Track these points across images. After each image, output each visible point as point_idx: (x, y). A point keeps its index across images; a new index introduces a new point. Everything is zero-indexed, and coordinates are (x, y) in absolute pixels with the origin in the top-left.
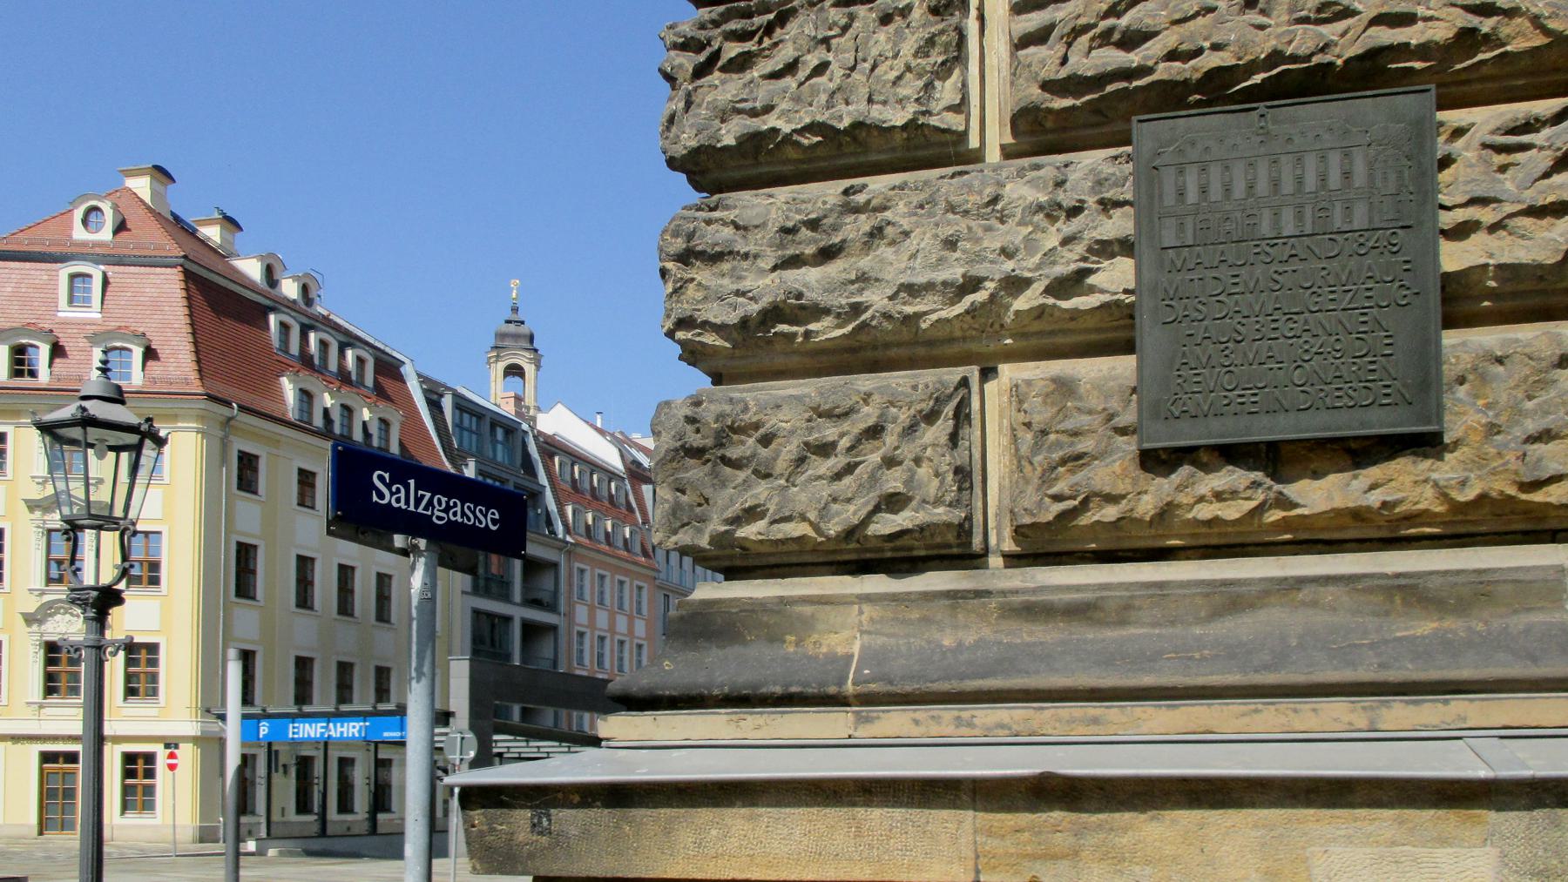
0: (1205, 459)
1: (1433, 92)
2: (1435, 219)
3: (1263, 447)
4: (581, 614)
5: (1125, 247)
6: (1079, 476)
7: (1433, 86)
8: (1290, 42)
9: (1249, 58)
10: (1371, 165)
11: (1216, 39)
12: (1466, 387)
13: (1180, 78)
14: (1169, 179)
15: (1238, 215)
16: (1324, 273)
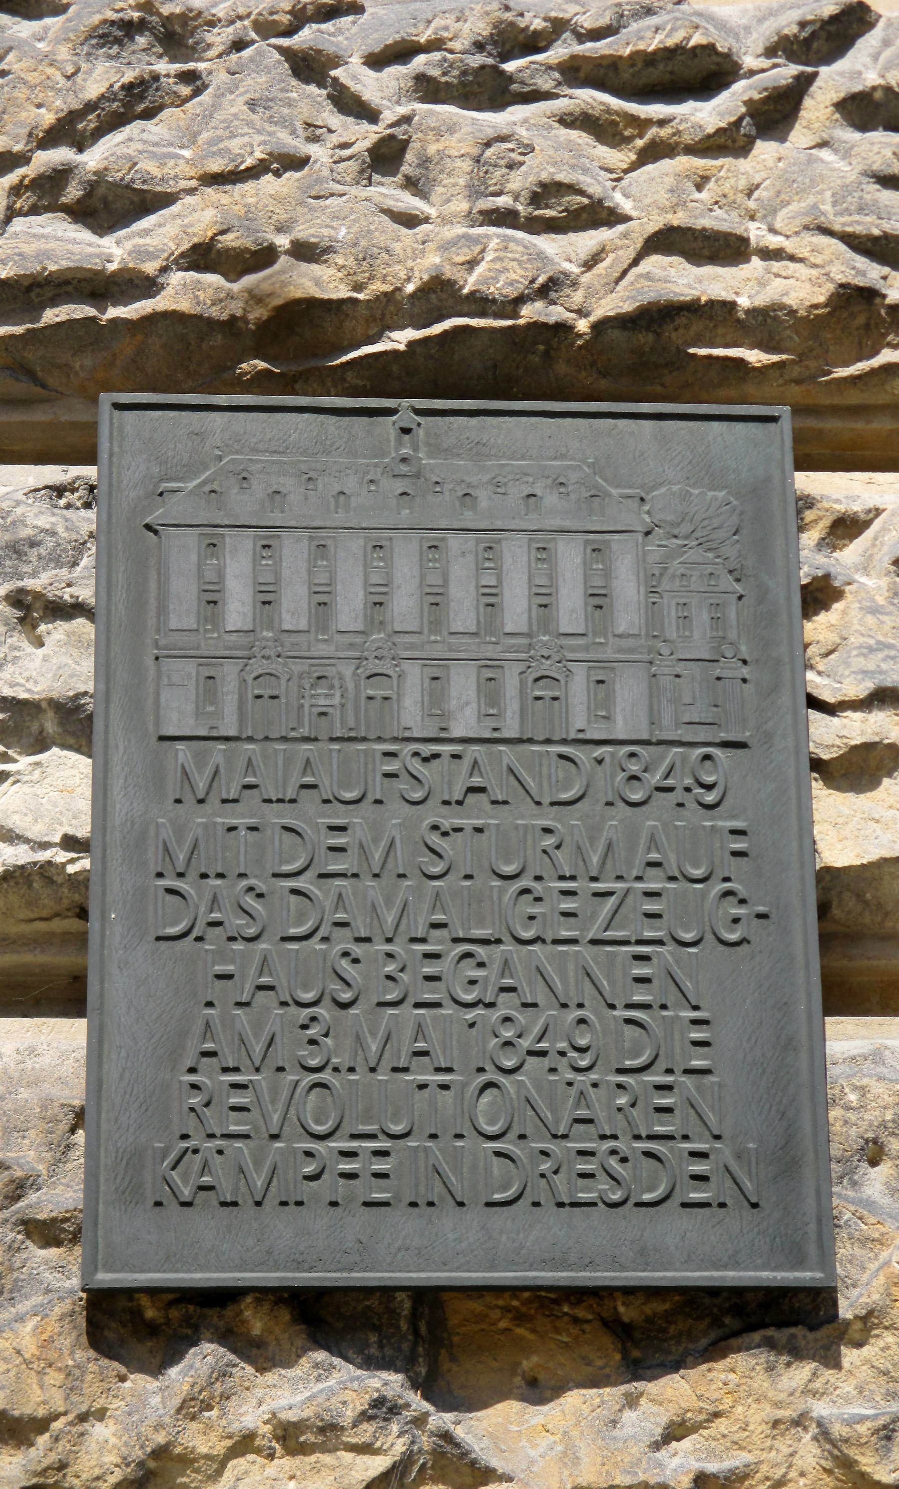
0: (257, 1327)
1: (786, 425)
2: (802, 732)
3: (405, 1304)
4: (339, 587)
5: (70, 723)
7: (784, 411)
8: (472, 264)
9: (378, 287)
11: (304, 232)
12: (885, 1169)
14: (183, 553)
15: (347, 670)
16: (549, 841)
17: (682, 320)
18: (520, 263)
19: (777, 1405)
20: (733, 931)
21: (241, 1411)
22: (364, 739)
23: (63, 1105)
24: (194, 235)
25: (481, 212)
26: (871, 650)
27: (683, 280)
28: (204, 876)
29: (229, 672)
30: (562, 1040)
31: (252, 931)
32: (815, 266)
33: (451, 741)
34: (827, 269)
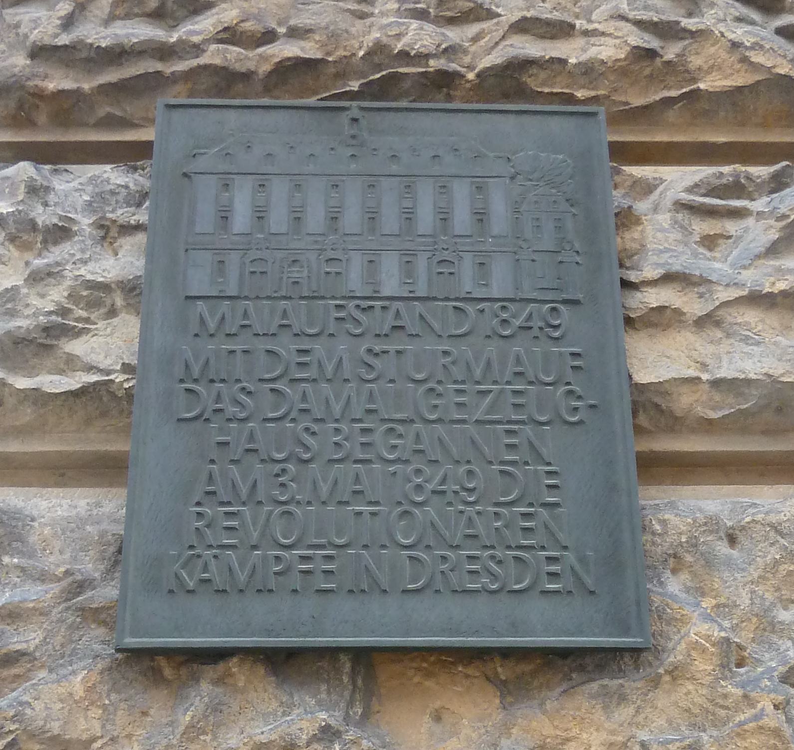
8: (399, 36)
9: (341, 53)
14: (206, 190)
15: (313, 256)
17: (534, 70)
18: (430, 36)
19: (613, 732)
20: (574, 416)
21: (228, 736)
22: (323, 298)
23: (114, 535)
24: (225, 22)
25: (406, 10)
26: (661, 252)
28: (212, 381)
29: (234, 258)
30: (456, 485)
31: (243, 415)
32: (617, 37)
33: (380, 299)
34: (625, 38)
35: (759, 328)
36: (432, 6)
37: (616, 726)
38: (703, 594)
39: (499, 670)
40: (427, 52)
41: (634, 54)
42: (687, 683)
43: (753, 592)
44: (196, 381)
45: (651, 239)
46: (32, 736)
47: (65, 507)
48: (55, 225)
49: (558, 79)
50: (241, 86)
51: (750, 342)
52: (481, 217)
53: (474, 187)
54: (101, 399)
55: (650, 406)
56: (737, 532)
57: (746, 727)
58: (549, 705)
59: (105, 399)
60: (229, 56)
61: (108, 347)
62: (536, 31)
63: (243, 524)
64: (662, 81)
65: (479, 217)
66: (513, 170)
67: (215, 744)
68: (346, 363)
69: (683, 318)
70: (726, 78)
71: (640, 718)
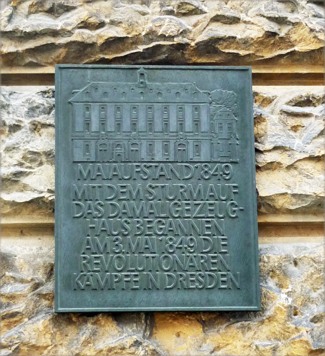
6: (13, 332)
9: (134, 33)
10: (211, 117)
13: (89, 41)
17: (221, 42)
18: (175, 26)
20: (234, 214)
22: (130, 162)
25: (164, 11)
26: (273, 136)
27: (221, 30)
29: (93, 143)
32: (259, 26)
34: (263, 27)
35: (313, 171)
36: (175, 7)
37: (247, 339)
38: (282, 287)
39: (202, 317)
40: (173, 35)
41: (266, 35)
42: (274, 322)
43: (302, 286)
44: (80, 200)
45: (270, 129)
46: (24, 344)
47: (28, 250)
48: (14, 124)
49: (232, 45)
50: (90, 49)
51: (308, 177)
52: (197, 123)
53: (194, 108)
54: (39, 203)
55: (264, 205)
56: (298, 260)
57: (295, 340)
58: (221, 331)
59: (41, 203)
60: (84, 36)
61: (41, 181)
62: (223, 21)
63: (102, 262)
64: (278, 46)
65: (196, 123)
66: (211, 99)
67: (94, 347)
68: (141, 193)
69: (281, 166)
70: (307, 45)
71: (256, 336)
